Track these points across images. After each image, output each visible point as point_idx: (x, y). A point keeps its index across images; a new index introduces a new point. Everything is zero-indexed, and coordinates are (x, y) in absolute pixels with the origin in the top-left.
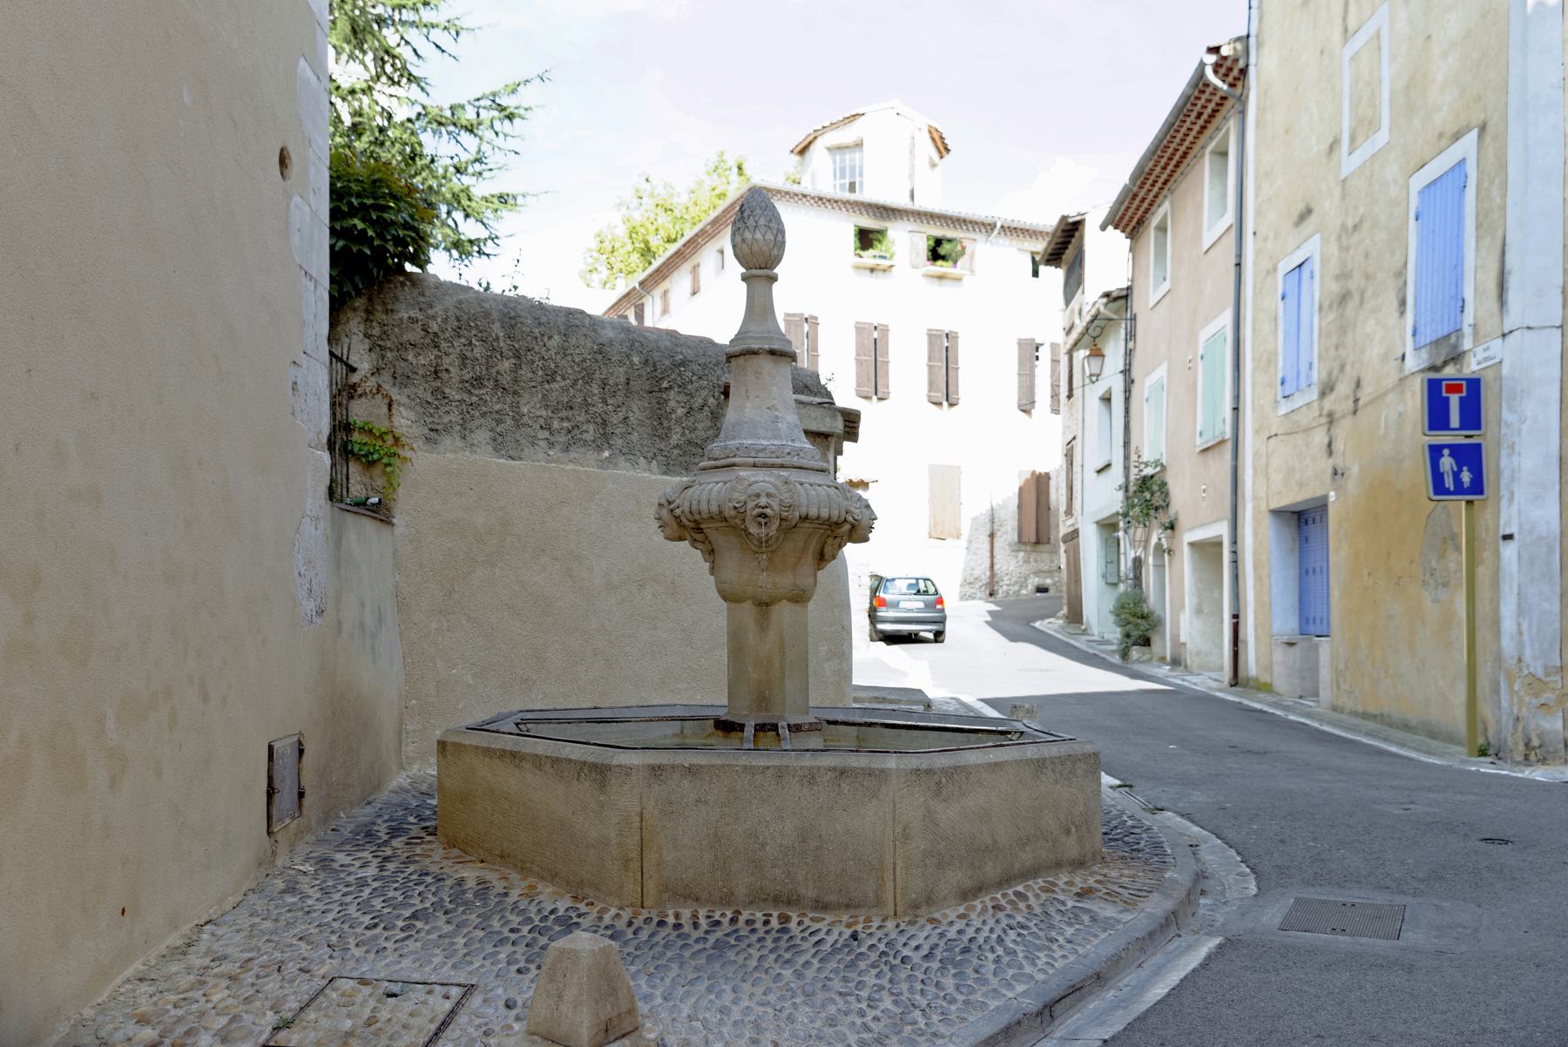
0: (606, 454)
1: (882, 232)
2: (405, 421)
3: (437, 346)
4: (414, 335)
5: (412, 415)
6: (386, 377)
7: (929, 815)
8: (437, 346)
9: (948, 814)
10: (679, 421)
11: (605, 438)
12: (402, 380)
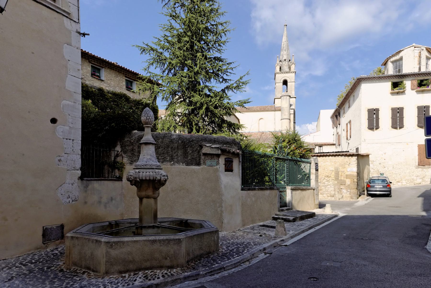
0: (172, 163)
1: (402, 82)
2: (125, 160)
3: (133, 145)
4: (128, 143)
5: (127, 159)
6: (122, 152)
7: (107, 252)
8: (133, 145)
9: (114, 253)
10: (190, 154)
11: (172, 159)
12: (125, 153)
